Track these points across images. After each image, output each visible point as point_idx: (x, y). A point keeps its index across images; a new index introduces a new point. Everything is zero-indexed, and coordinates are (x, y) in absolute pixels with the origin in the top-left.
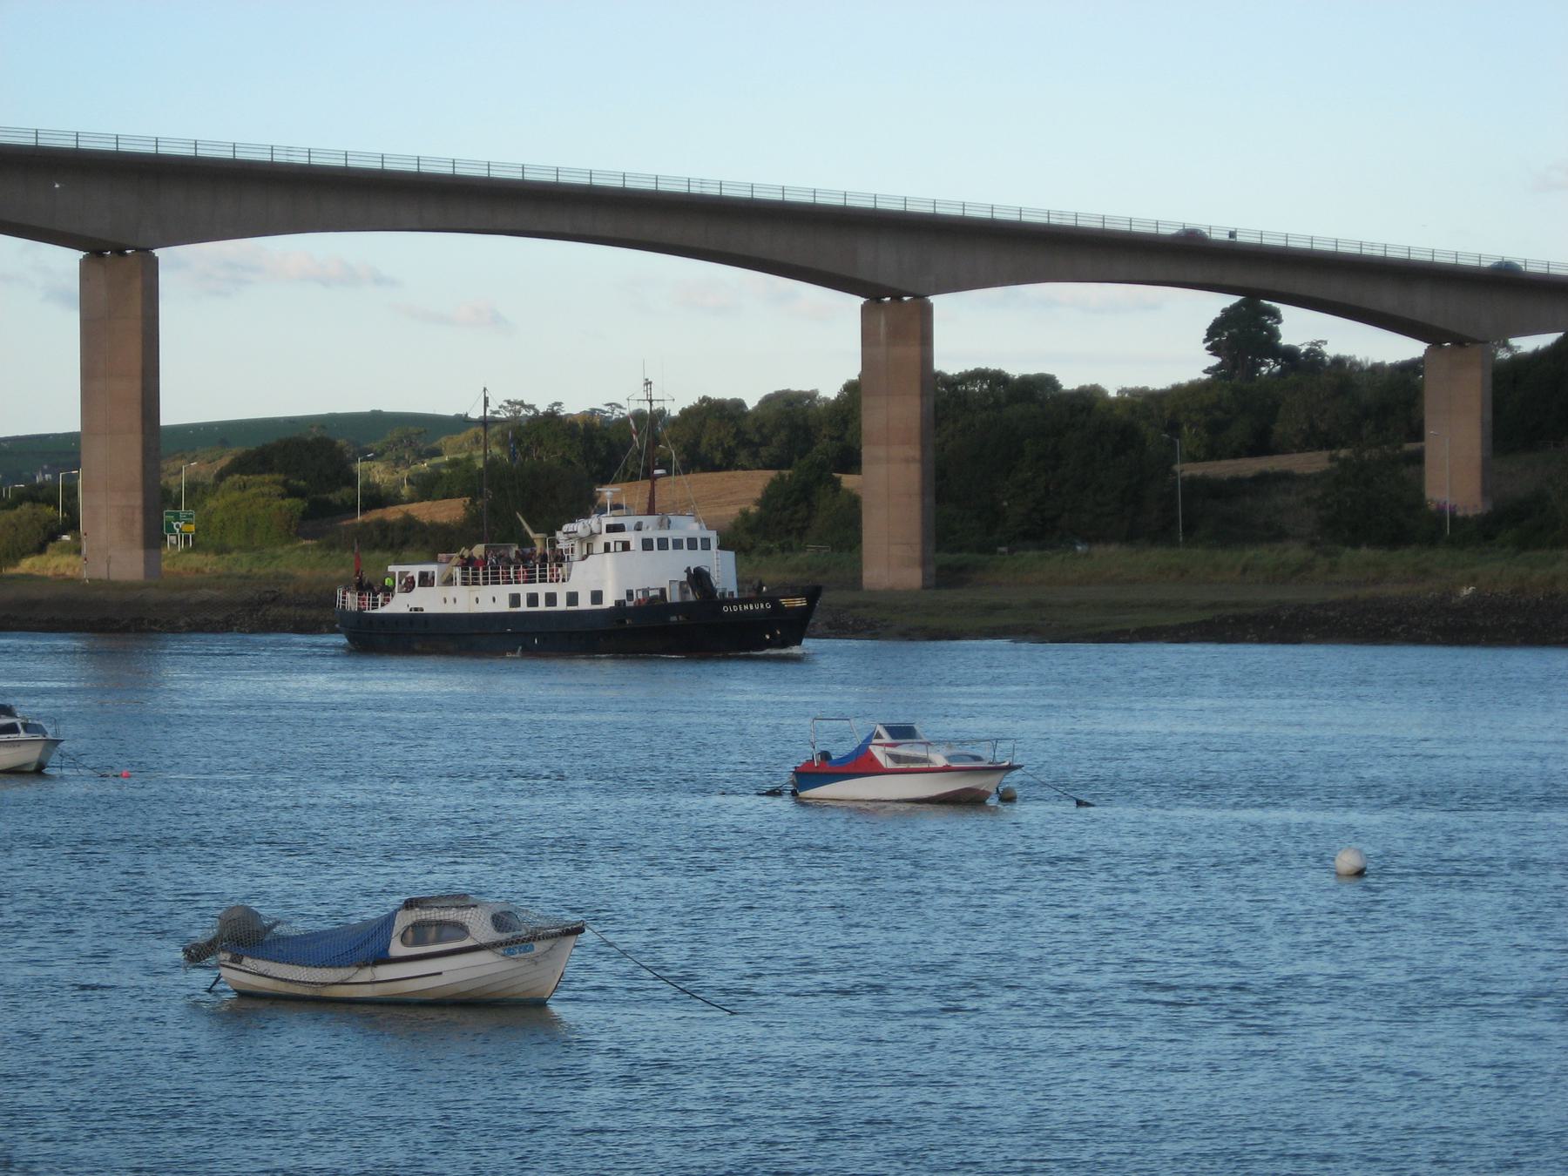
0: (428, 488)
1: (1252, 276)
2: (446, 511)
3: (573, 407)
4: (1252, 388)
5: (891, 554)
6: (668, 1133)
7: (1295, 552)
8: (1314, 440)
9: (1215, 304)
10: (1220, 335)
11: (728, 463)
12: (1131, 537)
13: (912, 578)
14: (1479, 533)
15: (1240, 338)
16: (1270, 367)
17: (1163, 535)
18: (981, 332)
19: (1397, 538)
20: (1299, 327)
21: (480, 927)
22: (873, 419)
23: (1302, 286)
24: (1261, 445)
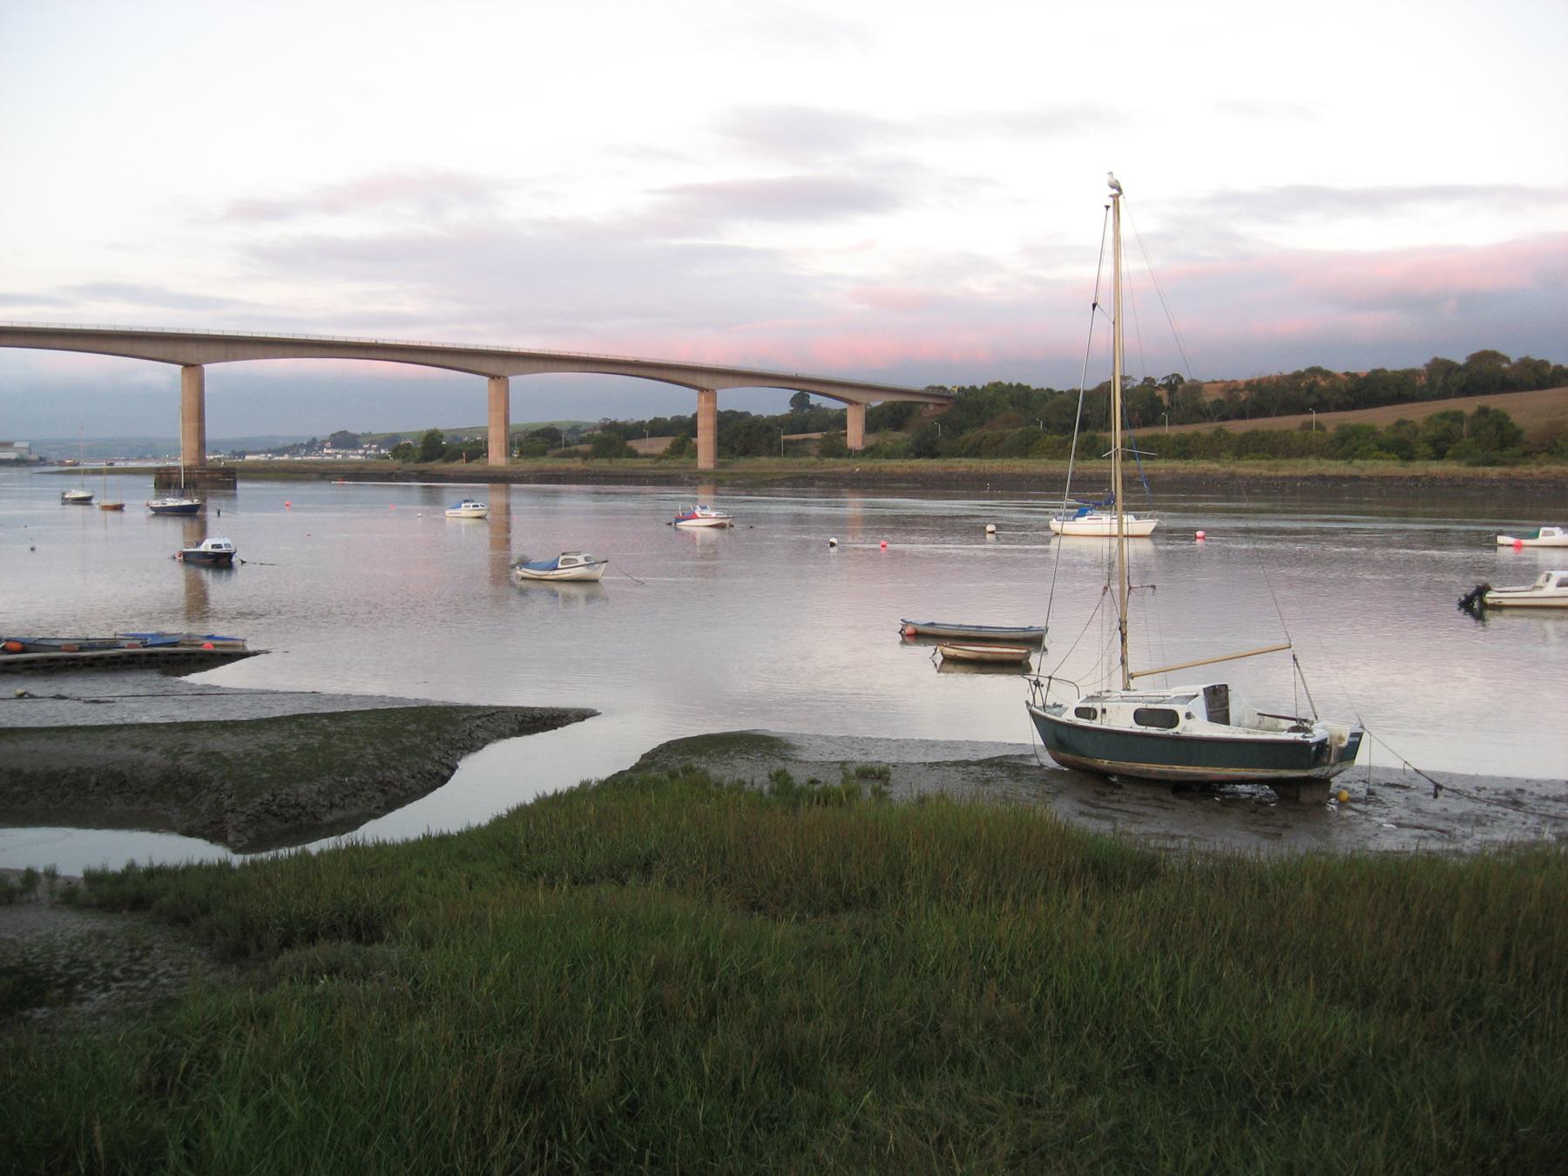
0: (582, 441)
1: (802, 385)
2: (586, 448)
3: (621, 420)
4: (803, 418)
5: (705, 456)
6: (150, 482)
7: (813, 459)
8: (819, 430)
9: (793, 393)
10: (793, 401)
11: (663, 435)
12: (770, 455)
13: (711, 466)
14: (870, 452)
15: (800, 401)
16: (807, 411)
17: (778, 454)
18: (734, 399)
19: (839, 456)
20: (814, 400)
21: (581, 560)
22: (701, 423)
23: (816, 388)
24: (804, 431)
